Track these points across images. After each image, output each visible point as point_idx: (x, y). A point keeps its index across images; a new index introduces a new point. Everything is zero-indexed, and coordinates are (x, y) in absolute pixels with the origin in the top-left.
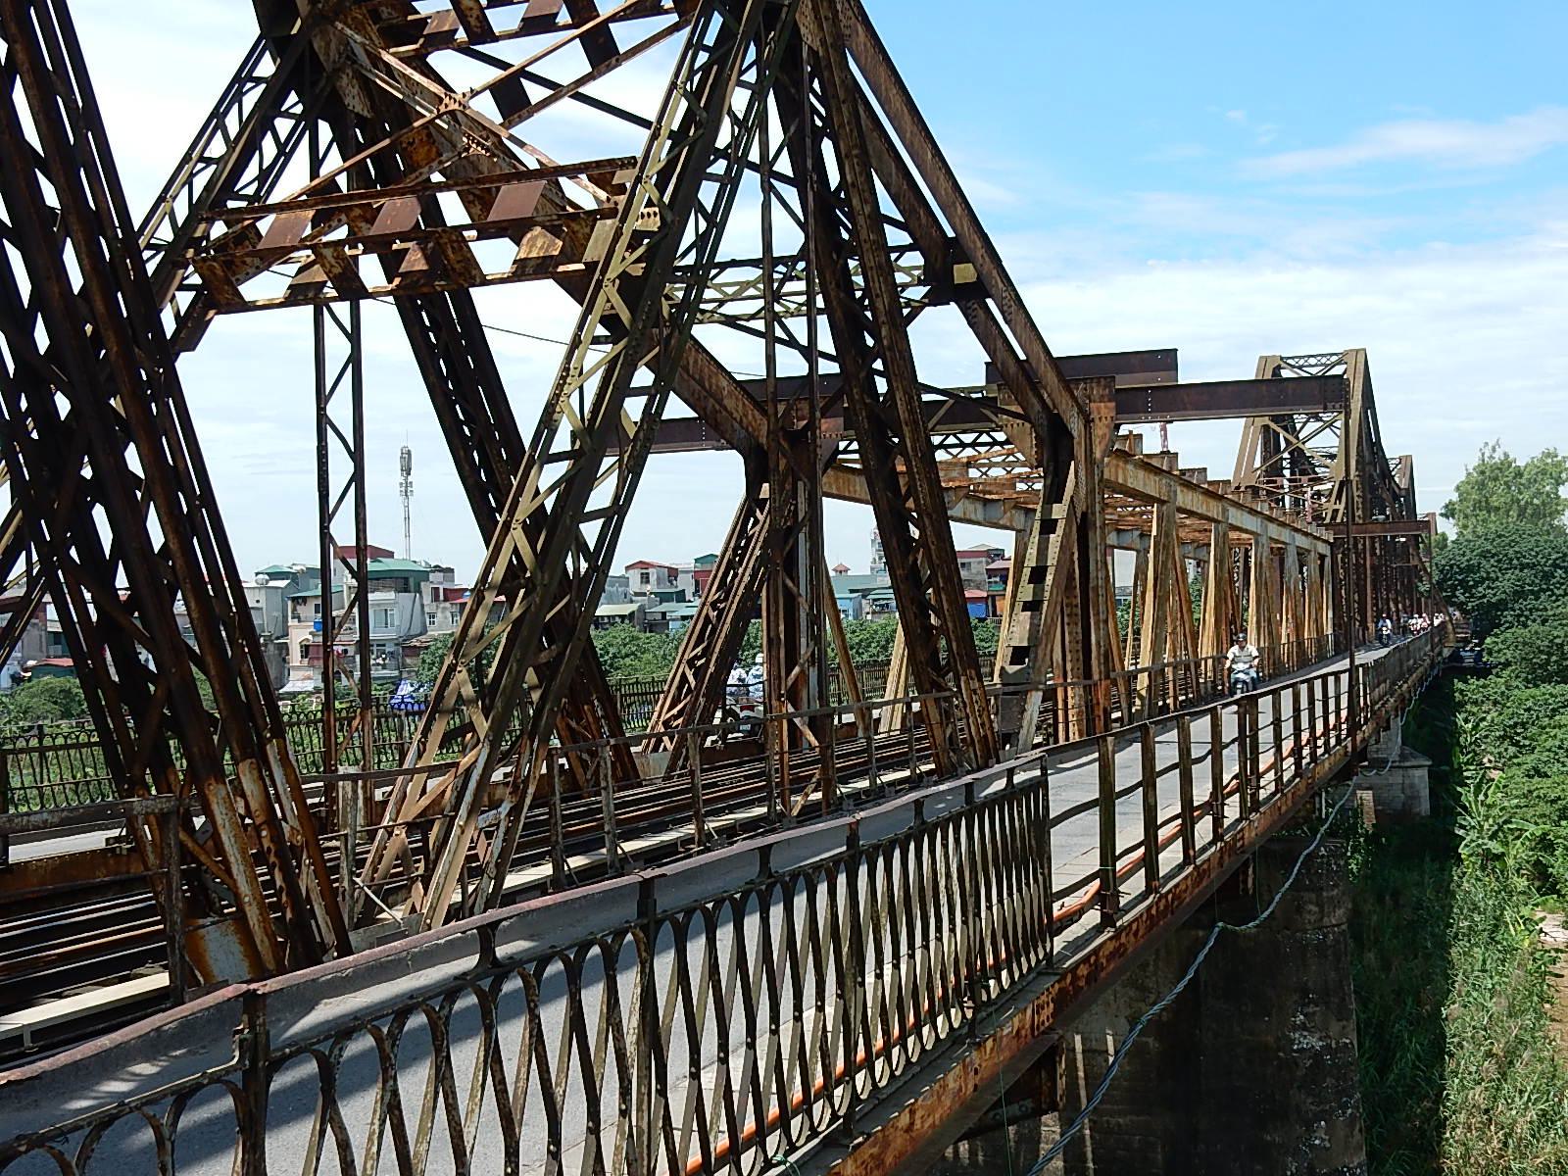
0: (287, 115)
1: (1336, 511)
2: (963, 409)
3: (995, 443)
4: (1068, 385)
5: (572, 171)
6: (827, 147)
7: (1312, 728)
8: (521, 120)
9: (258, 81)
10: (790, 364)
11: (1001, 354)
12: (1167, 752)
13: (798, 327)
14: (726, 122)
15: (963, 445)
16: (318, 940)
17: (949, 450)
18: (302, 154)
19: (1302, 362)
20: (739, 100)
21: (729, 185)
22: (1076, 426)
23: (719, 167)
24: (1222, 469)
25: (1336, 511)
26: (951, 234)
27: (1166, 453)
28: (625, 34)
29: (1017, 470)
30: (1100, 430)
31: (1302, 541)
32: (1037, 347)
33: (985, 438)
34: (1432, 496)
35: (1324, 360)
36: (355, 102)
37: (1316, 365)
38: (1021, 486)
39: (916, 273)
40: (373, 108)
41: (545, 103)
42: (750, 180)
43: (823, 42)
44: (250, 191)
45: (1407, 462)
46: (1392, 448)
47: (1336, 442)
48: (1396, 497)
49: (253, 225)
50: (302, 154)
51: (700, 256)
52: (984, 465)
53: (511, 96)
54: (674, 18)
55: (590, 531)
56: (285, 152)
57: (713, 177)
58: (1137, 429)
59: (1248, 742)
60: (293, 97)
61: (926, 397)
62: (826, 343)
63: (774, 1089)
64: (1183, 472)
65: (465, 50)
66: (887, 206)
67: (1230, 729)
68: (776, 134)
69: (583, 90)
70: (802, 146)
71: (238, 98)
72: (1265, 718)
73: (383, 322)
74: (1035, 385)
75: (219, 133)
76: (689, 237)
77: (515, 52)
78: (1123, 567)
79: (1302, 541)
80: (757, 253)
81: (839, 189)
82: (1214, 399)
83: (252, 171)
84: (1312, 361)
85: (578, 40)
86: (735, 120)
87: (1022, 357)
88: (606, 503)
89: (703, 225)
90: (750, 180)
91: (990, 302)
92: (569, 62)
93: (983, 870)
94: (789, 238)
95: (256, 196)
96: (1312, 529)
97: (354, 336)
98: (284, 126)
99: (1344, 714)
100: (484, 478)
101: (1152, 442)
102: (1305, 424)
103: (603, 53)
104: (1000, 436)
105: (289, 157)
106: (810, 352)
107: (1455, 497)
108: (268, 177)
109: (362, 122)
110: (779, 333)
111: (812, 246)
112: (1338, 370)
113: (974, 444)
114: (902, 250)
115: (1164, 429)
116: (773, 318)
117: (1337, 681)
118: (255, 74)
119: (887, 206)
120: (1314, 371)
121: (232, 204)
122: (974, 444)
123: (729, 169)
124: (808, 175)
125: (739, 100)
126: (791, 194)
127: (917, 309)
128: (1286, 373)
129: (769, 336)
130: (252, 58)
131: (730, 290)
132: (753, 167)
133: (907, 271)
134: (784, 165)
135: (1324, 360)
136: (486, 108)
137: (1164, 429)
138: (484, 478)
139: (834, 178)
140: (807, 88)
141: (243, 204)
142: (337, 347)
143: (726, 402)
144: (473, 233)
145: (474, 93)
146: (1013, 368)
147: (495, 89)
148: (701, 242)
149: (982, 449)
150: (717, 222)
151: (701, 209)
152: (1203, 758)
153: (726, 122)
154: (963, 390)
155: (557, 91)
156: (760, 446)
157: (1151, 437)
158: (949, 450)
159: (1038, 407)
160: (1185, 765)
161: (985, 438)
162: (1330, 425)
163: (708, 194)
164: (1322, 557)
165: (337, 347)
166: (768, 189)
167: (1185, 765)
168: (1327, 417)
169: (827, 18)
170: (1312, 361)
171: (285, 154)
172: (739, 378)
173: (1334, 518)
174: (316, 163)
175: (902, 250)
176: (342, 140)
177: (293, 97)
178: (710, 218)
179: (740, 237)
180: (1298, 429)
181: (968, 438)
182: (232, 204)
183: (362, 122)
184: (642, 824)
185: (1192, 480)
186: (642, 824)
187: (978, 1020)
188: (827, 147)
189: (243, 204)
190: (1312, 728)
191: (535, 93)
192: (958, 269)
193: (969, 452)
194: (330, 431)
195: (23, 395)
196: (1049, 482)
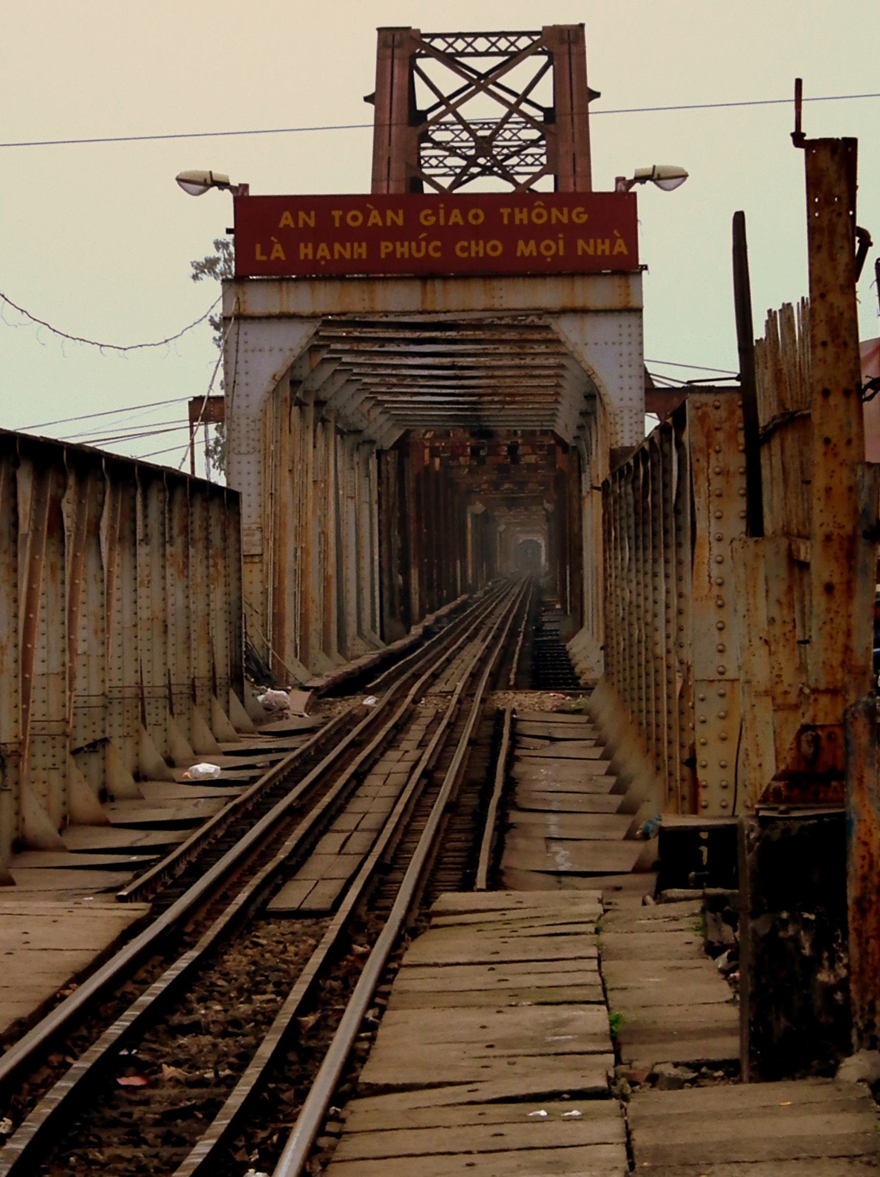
19: (460, 45)
35: (503, 44)
37: (487, 54)
84: (481, 44)
135: (503, 44)
170: (481, 44)
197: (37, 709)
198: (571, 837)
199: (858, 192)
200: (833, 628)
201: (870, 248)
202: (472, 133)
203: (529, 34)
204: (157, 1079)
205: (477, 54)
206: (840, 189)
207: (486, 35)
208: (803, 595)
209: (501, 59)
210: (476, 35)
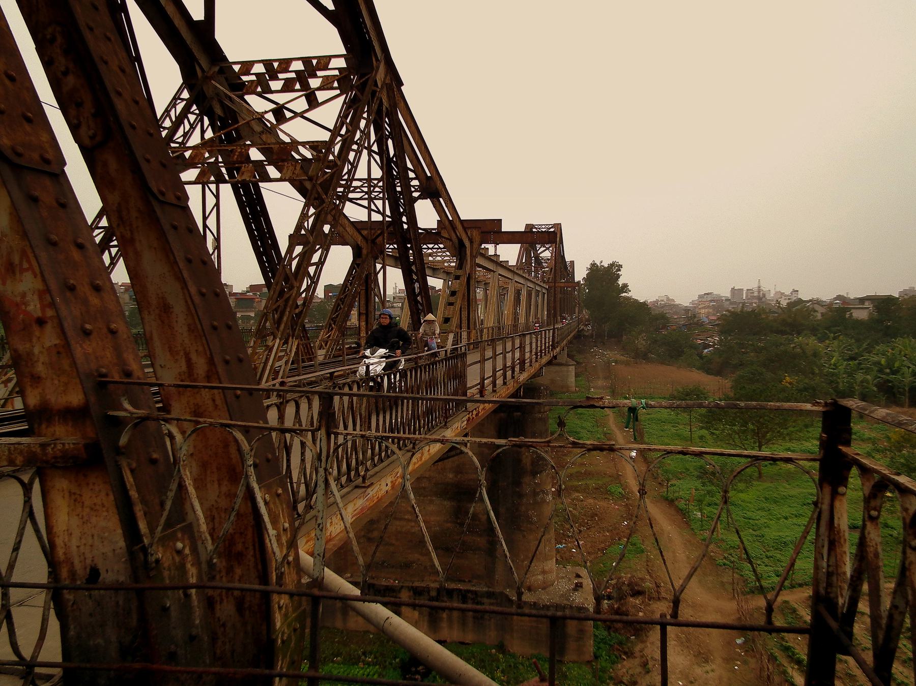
0: (193, 113)
2: (431, 236)
3: (440, 248)
4: (465, 229)
5: (304, 144)
6: (390, 142)
7: (541, 347)
8: (283, 123)
9: (183, 100)
10: (377, 217)
11: (444, 218)
12: (499, 349)
13: (379, 203)
14: (358, 132)
15: (428, 248)
17: (428, 249)
18: (198, 130)
20: (363, 123)
21: (359, 153)
22: (467, 244)
23: (355, 147)
24: (513, 262)
26: (429, 175)
27: (496, 255)
28: (321, 96)
29: (446, 258)
30: (475, 246)
31: (538, 288)
32: (456, 216)
33: (436, 246)
34: (580, 274)
36: (218, 111)
38: (446, 264)
39: (417, 187)
40: (225, 113)
41: (291, 118)
42: (365, 152)
43: (390, 105)
44: (180, 140)
45: (572, 263)
46: (568, 258)
47: (550, 255)
48: (568, 275)
49: (183, 153)
50: (198, 130)
51: (349, 176)
52: (434, 256)
53: (279, 112)
54: (338, 92)
55: (312, 270)
56: (193, 127)
57: (353, 150)
58: (487, 246)
59: (522, 348)
60: (194, 107)
61: (420, 231)
62: (388, 212)
63: (369, 447)
64: (501, 262)
65: (260, 95)
66: (409, 165)
67: (517, 344)
68: (373, 137)
69: (305, 115)
70: (381, 142)
71: (175, 106)
72: (528, 342)
73: (226, 190)
74: (454, 228)
75: (168, 118)
76: (346, 170)
77: (281, 98)
78: (479, 293)
79: (538, 288)
81: (393, 157)
82: (511, 238)
83: (180, 132)
84: (543, 227)
85: (304, 97)
86: (361, 131)
87: (451, 219)
88: (317, 261)
89: (350, 167)
90: (365, 152)
91: (441, 199)
92: (301, 104)
94: (377, 173)
95: (182, 143)
96: (542, 284)
97: (217, 197)
98: (192, 118)
99: (551, 343)
101: (491, 252)
103: (313, 103)
104: (442, 246)
105: (194, 129)
106: (383, 214)
107: (585, 276)
108: (186, 135)
109: (220, 119)
110: (373, 207)
111: (385, 177)
112: (552, 230)
113: (433, 248)
114: (412, 179)
115: (496, 247)
116: (371, 200)
117: (549, 332)
118: (181, 97)
119: (409, 165)
120: (544, 230)
121: (173, 145)
122: (433, 248)
123: (358, 148)
124: (383, 151)
125: (363, 123)
126: (377, 158)
127: (416, 199)
128: (534, 230)
129: (369, 208)
130: (180, 91)
131: (358, 190)
132: (366, 148)
133: (414, 186)
134: (375, 148)
136: (270, 117)
137: (496, 247)
139: (392, 152)
140: (383, 121)
141: (178, 145)
142: (211, 201)
143: (347, 229)
144: (266, 163)
145: (266, 112)
146: (447, 223)
147: (273, 111)
148: (349, 172)
149: (435, 250)
150: (354, 166)
151: (349, 162)
152: (509, 352)
153: (358, 132)
154: (429, 229)
155: (296, 115)
156: (358, 245)
157: (491, 249)
158: (428, 249)
159: (455, 237)
160: (504, 353)
161: (436, 246)
162: (548, 249)
163: (352, 156)
164: (544, 293)
165: (211, 201)
166: (370, 155)
167: (504, 353)
168: (547, 246)
170: (543, 227)
171: (193, 128)
172: (352, 220)
174: (203, 132)
175: (412, 179)
176: (212, 124)
177: (194, 107)
178: (352, 164)
179: (361, 173)
181: (430, 246)
182: (173, 145)
183: (220, 119)
185: (503, 265)
187: (368, 476)
188: (390, 142)
189: (178, 145)
190: (541, 347)
191: (288, 115)
193: (430, 251)
194: (207, 230)
196: (458, 262)
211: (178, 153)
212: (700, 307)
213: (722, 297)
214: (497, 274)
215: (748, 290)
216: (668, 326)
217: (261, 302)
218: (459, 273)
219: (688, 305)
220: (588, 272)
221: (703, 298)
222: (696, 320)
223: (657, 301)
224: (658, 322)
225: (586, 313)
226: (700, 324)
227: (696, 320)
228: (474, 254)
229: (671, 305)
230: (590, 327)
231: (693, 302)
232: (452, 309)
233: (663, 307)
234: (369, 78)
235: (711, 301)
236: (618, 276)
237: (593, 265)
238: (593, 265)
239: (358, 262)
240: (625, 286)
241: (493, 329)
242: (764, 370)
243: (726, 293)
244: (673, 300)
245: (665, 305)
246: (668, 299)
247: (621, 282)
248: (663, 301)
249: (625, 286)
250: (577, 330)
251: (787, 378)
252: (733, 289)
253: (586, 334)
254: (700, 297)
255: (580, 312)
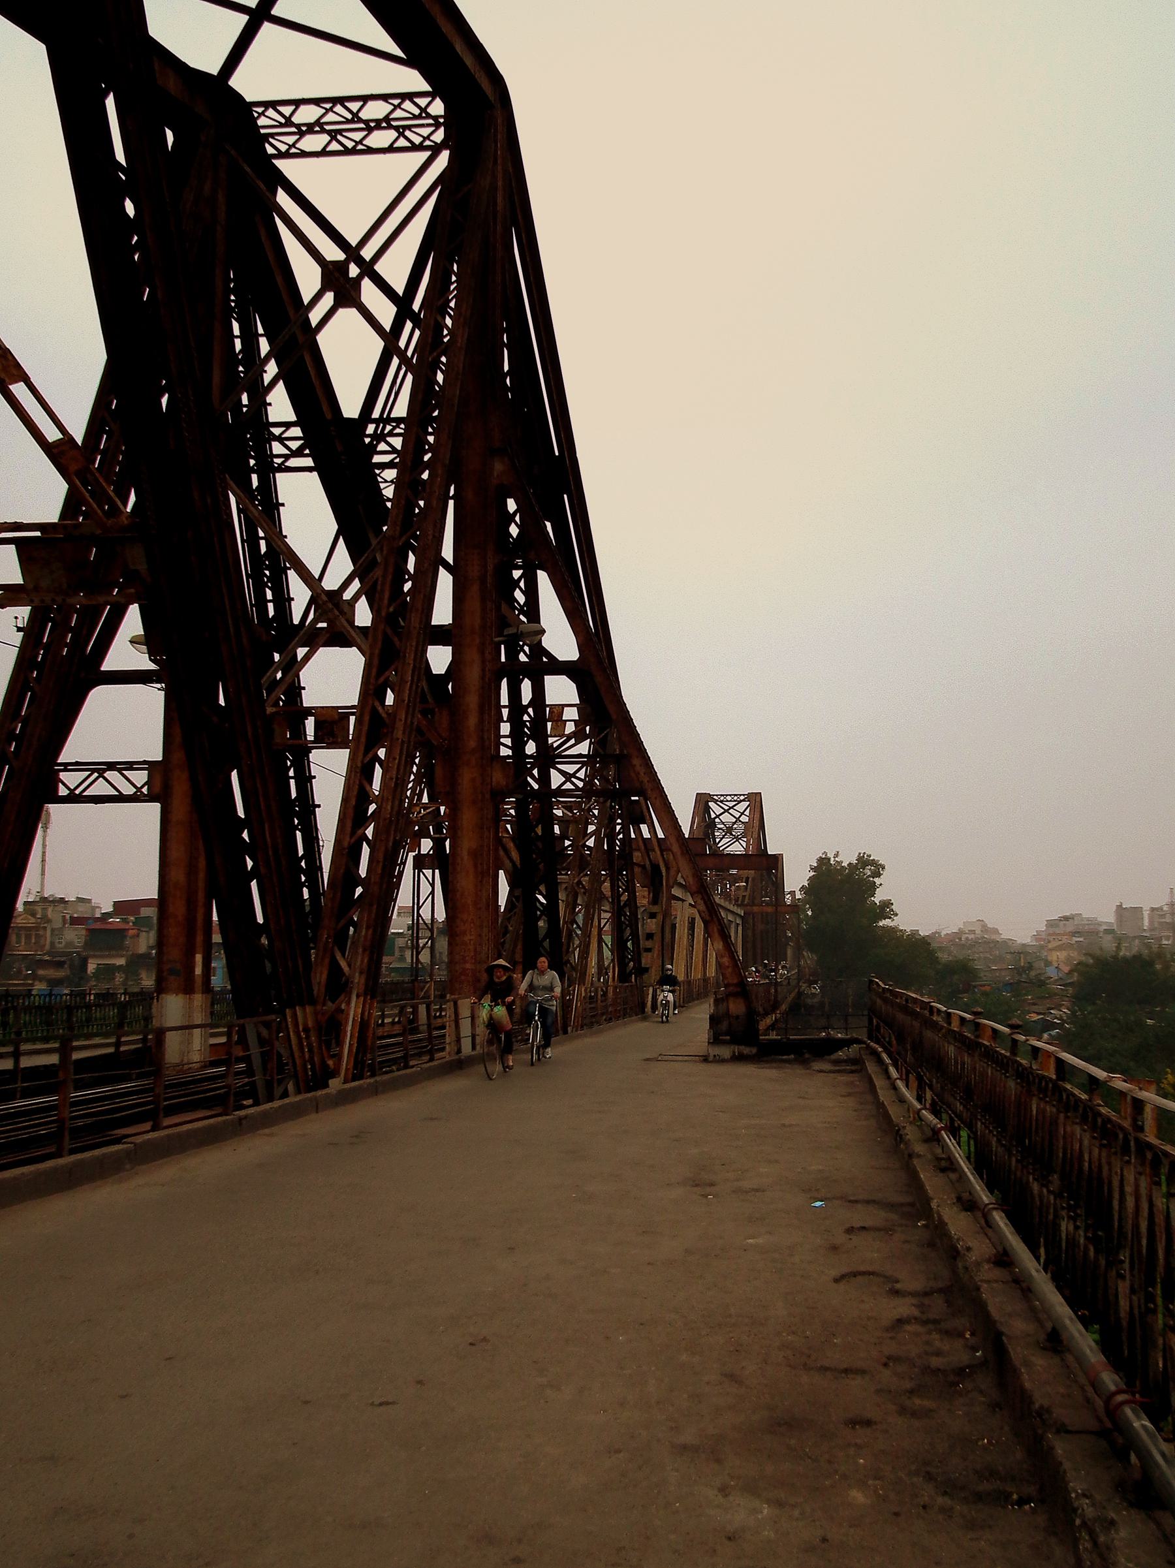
1: (744, 897)
16: (318, 864)
19: (722, 798)
25: (744, 897)
35: (736, 798)
37: (731, 801)
80: (379, 267)
84: (729, 798)
93: (396, 383)
100: (509, 394)
102: (721, 839)
135: (736, 798)
138: (509, 394)
169: (1116, 1173)
170: (729, 798)
173: (743, 900)
180: (717, 842)
184: (420, 649)
186: (420, 649)
192: (503, 725)
195: (518, 514)
197: (608, 910)
198: (272, 117)
199: (374, 93)
200: (836, 1471)
201: (293, 603)
202: (725, 825)
203: (744, 795)
204: (495, 1059)
205: (727, 801)
206: (25, 376)
207: (730, 795)
208: (696, 1061)
209: (735, 803)
210: (727, 795)
211: (431, 809)
212: (1050, 946)
213: (1100, 924)
214: (686, 904)
215: (1153, 909)
216: (975, 987)
217: (138, 936)
218: (655, 909)
219: (1027, 940)
220: (812, 874)
221: (1057, 926)
222: (1033, 973)
223: (961, 932)
224: (956, 977)
225: (809, 959)
226: (1041, 983)
227: (1033, 973)
228: (671, 884)
229: (989, 942)
230: (816, 989)
231: (1036, 937)
232: (649, 956)
233: (971, 947)
234: (607, 733)
235: (1074, 934)
236: (873, 888)
237: (823, 861)
238: (823, 861)
239: (516, 894)
240: (887, 904)
241: (684, 983)
242: (1132, 1064)
243: (1107, 917)
244: (996, 931)
245: (976, 943)
246: (985, 928)
247: (878, 898)
248: (973, 932)
249: (887, 904)
250: (797, 990)
251: (1169, 1076)
252: (1120, 907)
253: (809, 1001)
254: (1051, 924)
255: (798, 956)
